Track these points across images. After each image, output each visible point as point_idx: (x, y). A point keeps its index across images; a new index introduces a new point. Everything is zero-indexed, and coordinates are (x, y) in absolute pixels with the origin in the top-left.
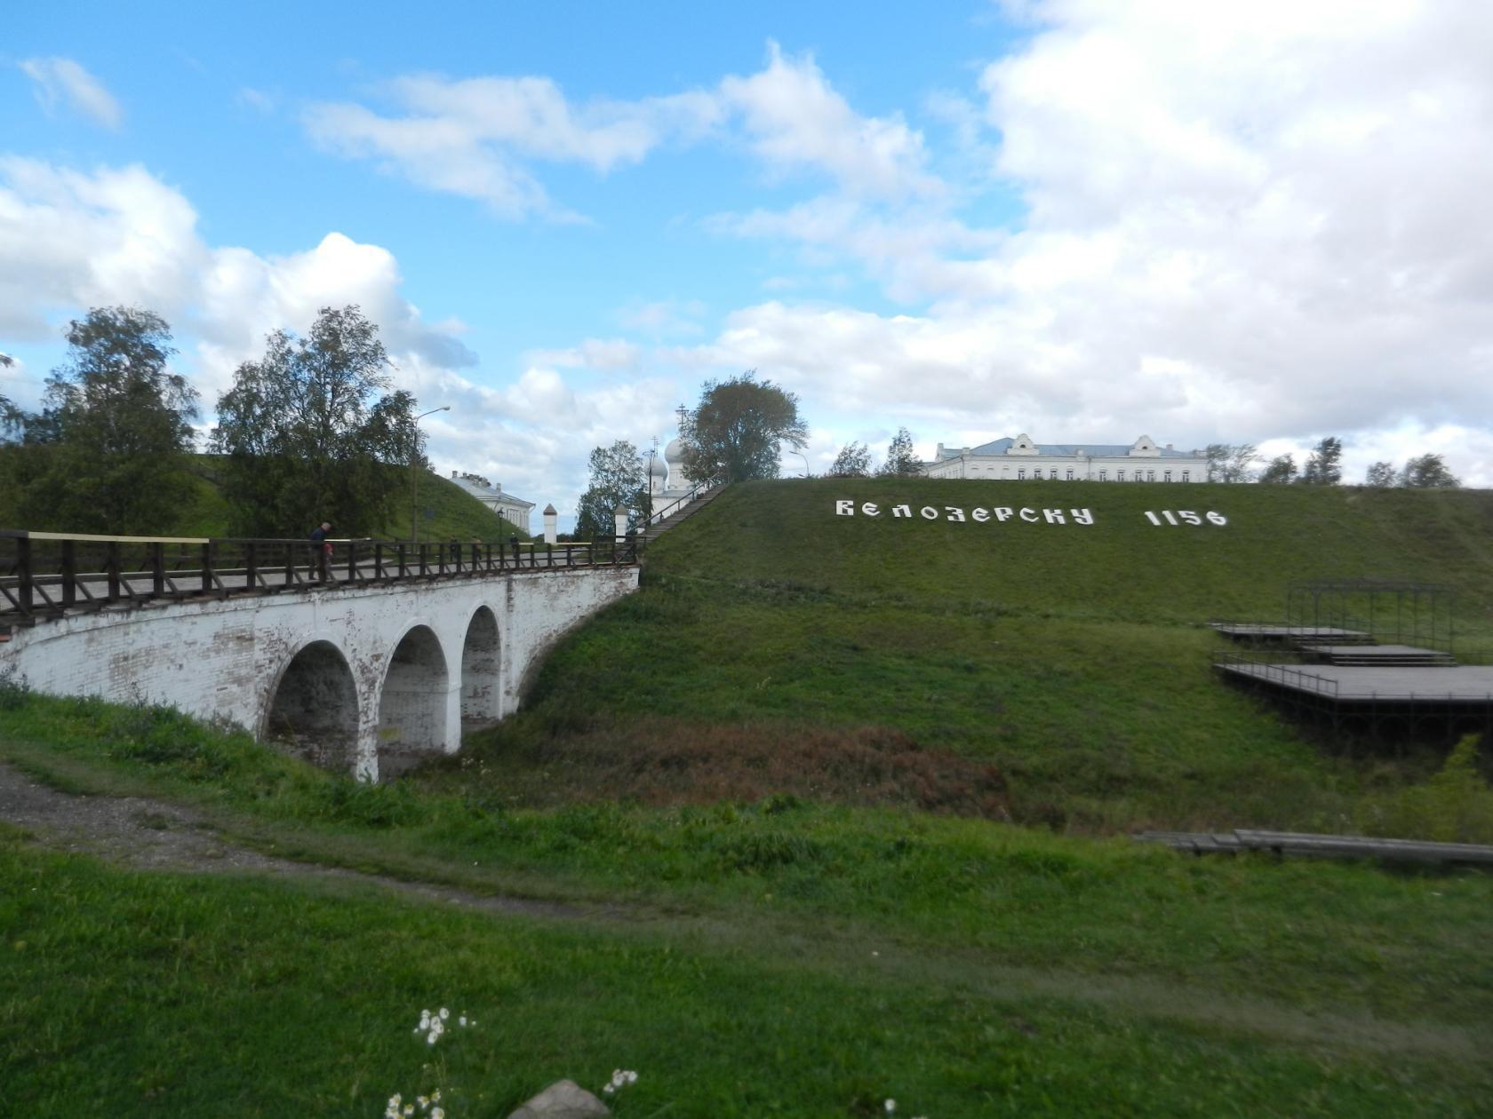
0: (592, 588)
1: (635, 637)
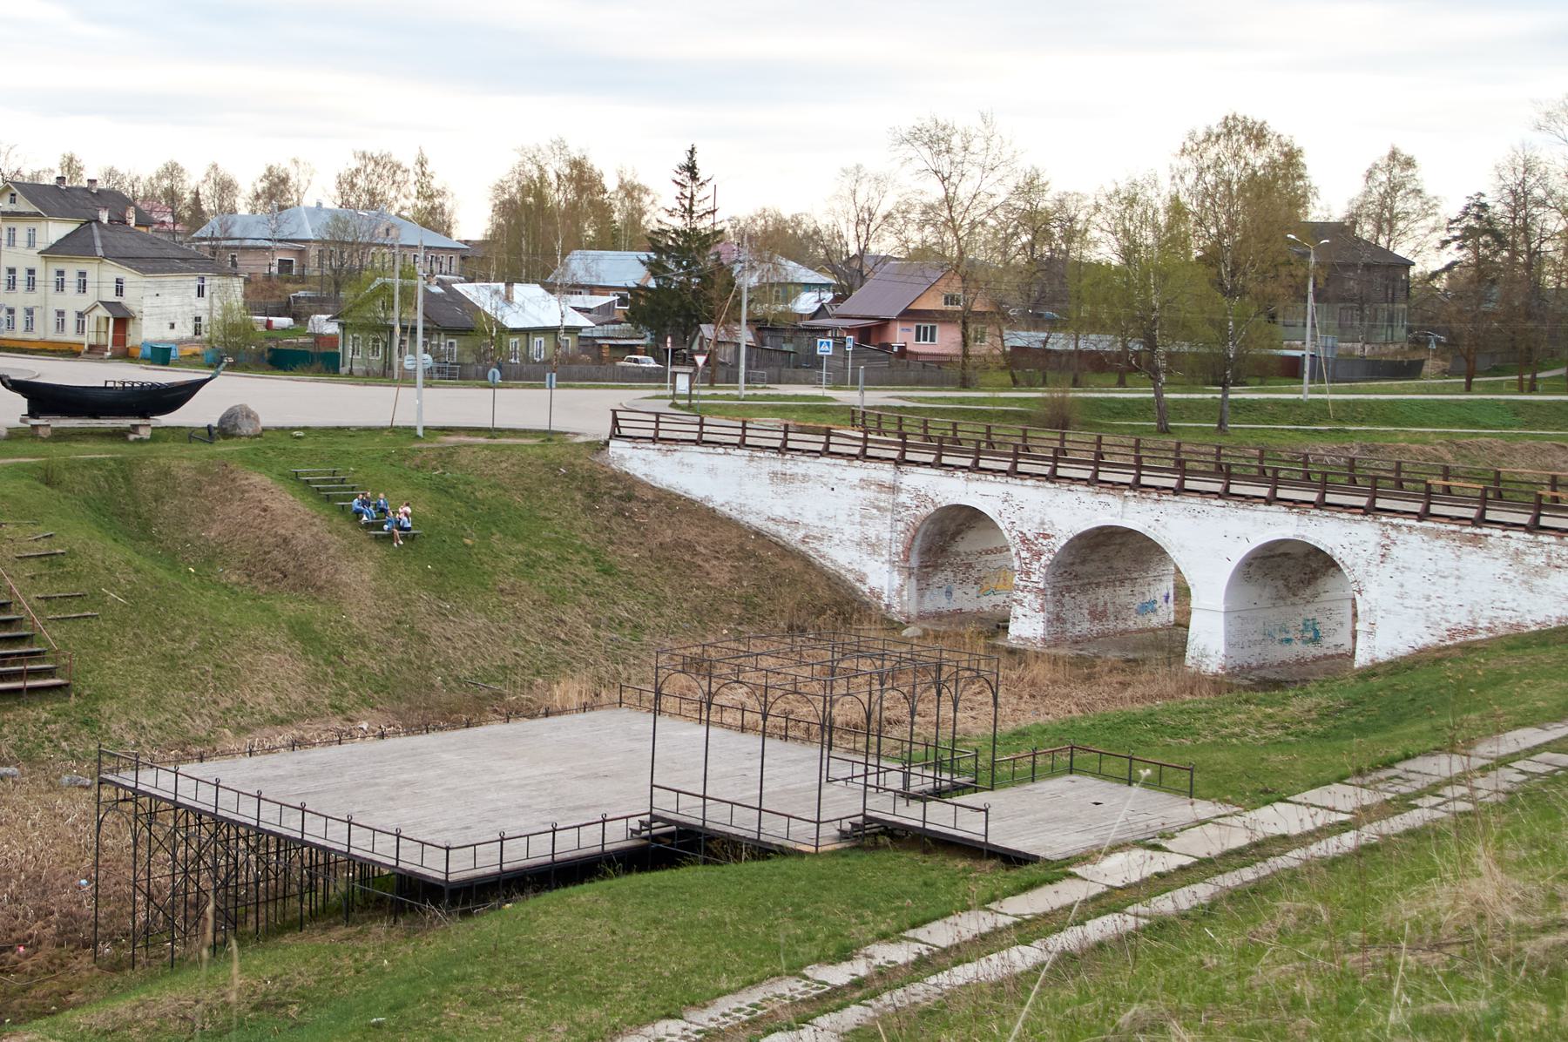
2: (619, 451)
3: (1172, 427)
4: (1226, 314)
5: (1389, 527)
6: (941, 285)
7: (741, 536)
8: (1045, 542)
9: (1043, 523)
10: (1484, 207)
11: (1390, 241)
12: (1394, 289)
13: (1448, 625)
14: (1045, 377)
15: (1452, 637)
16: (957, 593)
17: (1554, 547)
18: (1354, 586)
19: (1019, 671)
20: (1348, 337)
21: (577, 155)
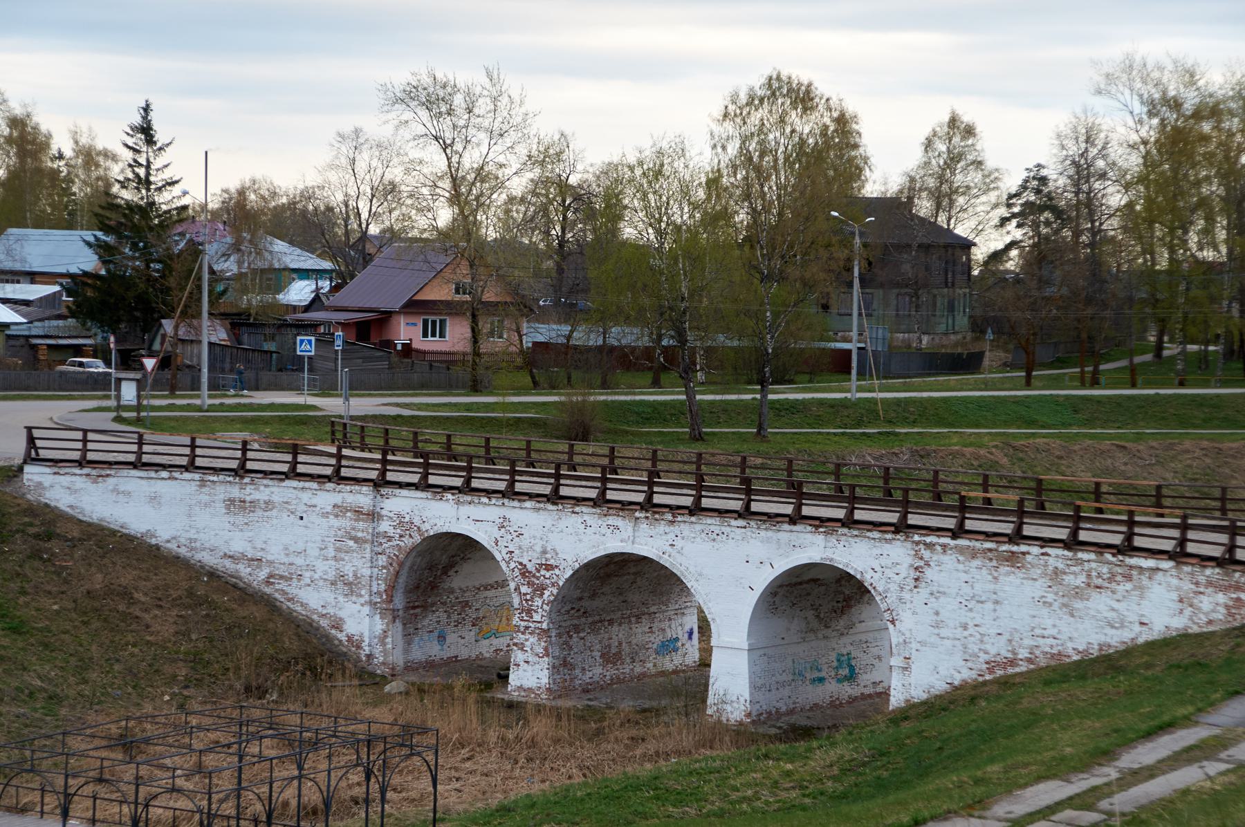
0: (1175, 596)
2: (37, 478)
3: (706, 433)
4: (762, 304)
5: (922, 546)
6: (447, 274)
7: (190, 579)
8: (548, 575)
10: (1043, 180)
11: (949, 219)
12: (953, 272)
13: (987, 657)
14: (569, 378)
15: (991, 671)
16: (451, 638)
17: (1094, 565)
18: (887, 615)
19: (517, 730)
20: (903, 327)
21: (18, 111)
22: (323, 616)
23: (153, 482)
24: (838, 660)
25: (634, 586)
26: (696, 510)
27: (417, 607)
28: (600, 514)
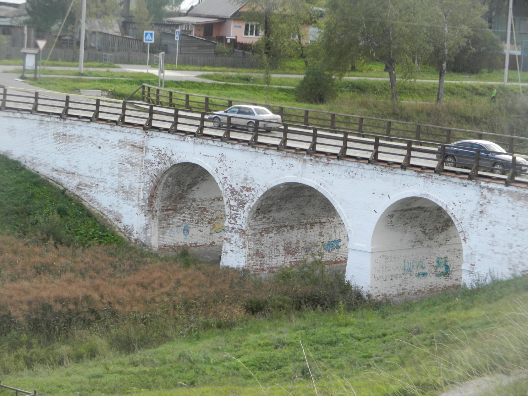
1: (165, 271)
8: (247, 194)
9: (246, 179)
16: (193, 231)
22: (110, 212)
23: (11, 119)
24: (438, 262)
25: (310, 204)
26: (342, 156)
27: (170, 210)
28: (281, 156)
